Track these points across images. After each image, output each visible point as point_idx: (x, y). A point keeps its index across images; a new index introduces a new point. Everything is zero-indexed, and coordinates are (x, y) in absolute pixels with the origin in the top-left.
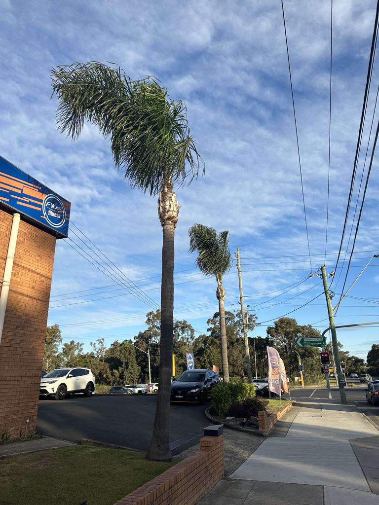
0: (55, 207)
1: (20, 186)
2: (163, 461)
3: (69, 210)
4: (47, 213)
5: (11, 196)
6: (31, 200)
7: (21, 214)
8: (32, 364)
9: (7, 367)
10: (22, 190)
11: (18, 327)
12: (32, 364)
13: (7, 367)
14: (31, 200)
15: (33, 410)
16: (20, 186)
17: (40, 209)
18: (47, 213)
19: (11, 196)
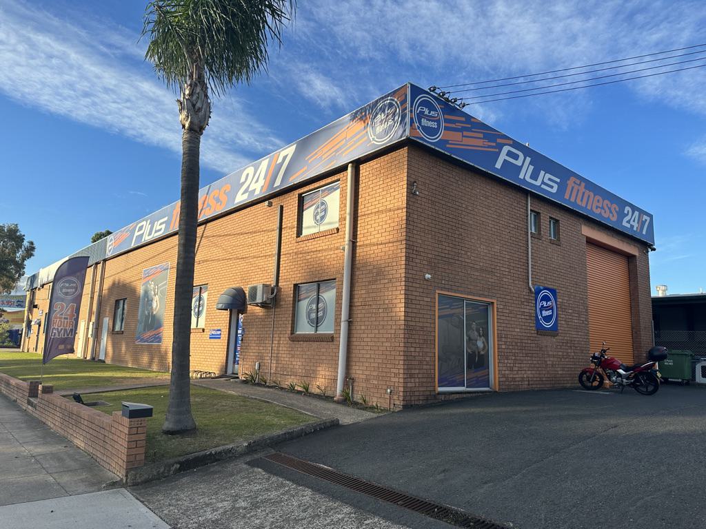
0: (429, 113)
1: (466, 141)
2: (377, 102)
3: (202, 129)
4: (420, 123)
5: (470, 126)
6: (454, 126)
7: (59, 344)
8: (390, 323)
9: (363, 327)
10: (463, 136)
11: (370, 282)
12: (390, 323)
13: (363, 327)
14: (454, 126)
15: (397, 380)
16: (466, 141)
17: (446, 116)
18: (420, 123)
19: (470, 126)
